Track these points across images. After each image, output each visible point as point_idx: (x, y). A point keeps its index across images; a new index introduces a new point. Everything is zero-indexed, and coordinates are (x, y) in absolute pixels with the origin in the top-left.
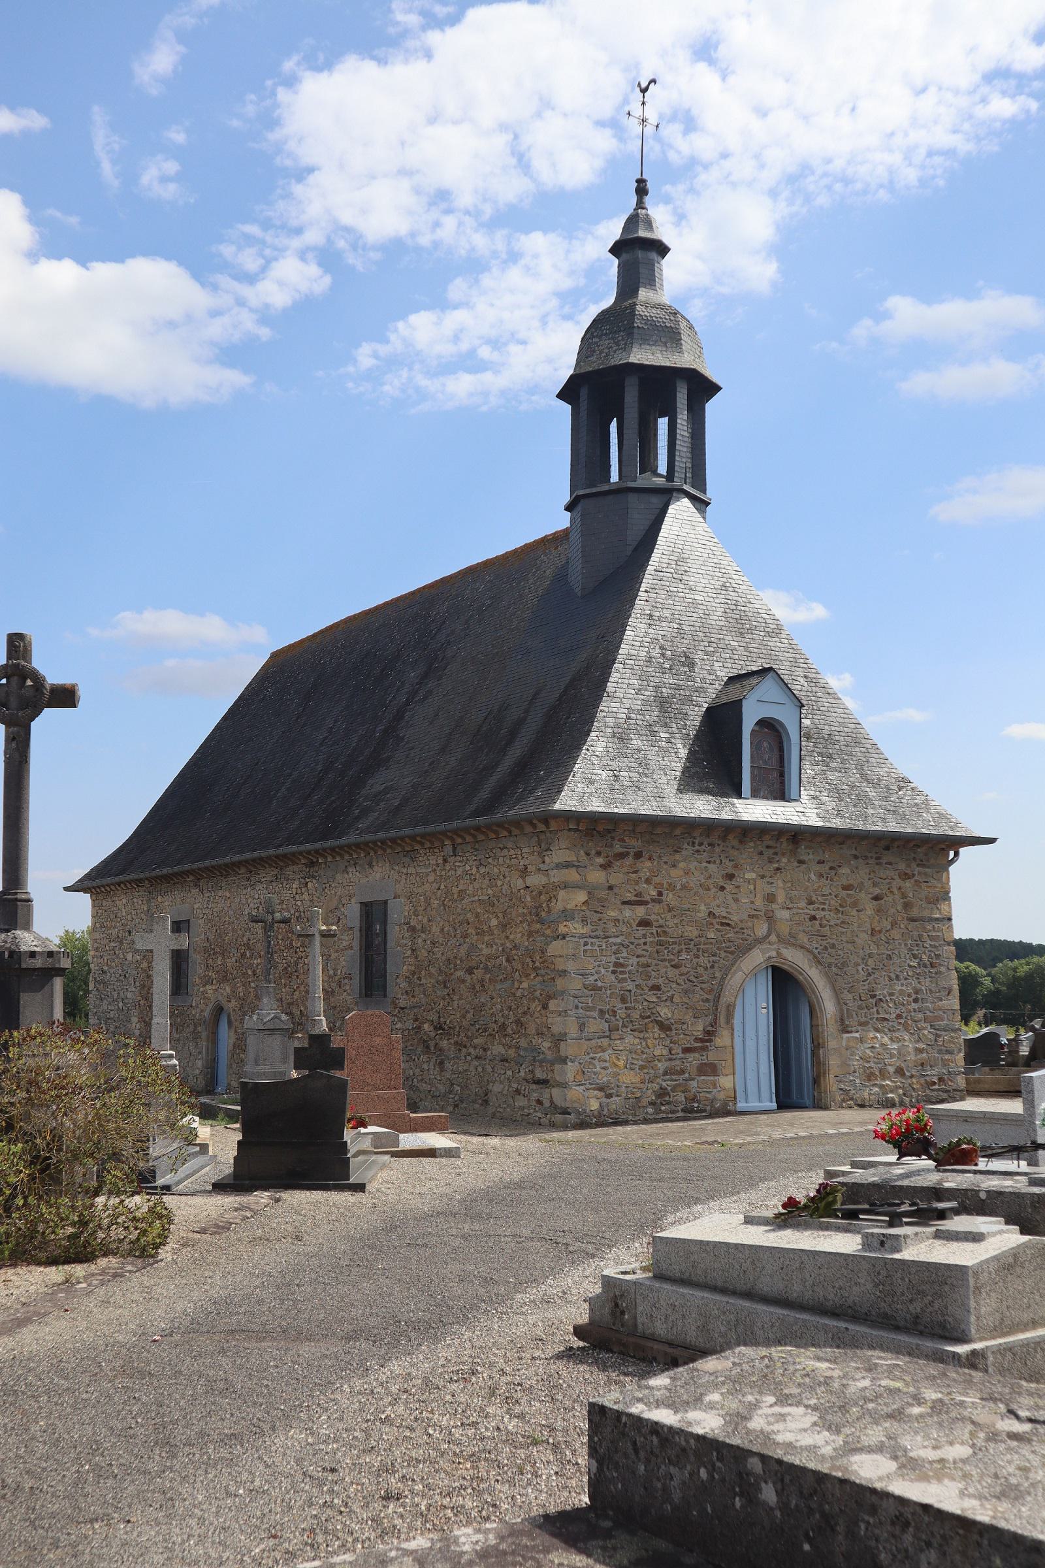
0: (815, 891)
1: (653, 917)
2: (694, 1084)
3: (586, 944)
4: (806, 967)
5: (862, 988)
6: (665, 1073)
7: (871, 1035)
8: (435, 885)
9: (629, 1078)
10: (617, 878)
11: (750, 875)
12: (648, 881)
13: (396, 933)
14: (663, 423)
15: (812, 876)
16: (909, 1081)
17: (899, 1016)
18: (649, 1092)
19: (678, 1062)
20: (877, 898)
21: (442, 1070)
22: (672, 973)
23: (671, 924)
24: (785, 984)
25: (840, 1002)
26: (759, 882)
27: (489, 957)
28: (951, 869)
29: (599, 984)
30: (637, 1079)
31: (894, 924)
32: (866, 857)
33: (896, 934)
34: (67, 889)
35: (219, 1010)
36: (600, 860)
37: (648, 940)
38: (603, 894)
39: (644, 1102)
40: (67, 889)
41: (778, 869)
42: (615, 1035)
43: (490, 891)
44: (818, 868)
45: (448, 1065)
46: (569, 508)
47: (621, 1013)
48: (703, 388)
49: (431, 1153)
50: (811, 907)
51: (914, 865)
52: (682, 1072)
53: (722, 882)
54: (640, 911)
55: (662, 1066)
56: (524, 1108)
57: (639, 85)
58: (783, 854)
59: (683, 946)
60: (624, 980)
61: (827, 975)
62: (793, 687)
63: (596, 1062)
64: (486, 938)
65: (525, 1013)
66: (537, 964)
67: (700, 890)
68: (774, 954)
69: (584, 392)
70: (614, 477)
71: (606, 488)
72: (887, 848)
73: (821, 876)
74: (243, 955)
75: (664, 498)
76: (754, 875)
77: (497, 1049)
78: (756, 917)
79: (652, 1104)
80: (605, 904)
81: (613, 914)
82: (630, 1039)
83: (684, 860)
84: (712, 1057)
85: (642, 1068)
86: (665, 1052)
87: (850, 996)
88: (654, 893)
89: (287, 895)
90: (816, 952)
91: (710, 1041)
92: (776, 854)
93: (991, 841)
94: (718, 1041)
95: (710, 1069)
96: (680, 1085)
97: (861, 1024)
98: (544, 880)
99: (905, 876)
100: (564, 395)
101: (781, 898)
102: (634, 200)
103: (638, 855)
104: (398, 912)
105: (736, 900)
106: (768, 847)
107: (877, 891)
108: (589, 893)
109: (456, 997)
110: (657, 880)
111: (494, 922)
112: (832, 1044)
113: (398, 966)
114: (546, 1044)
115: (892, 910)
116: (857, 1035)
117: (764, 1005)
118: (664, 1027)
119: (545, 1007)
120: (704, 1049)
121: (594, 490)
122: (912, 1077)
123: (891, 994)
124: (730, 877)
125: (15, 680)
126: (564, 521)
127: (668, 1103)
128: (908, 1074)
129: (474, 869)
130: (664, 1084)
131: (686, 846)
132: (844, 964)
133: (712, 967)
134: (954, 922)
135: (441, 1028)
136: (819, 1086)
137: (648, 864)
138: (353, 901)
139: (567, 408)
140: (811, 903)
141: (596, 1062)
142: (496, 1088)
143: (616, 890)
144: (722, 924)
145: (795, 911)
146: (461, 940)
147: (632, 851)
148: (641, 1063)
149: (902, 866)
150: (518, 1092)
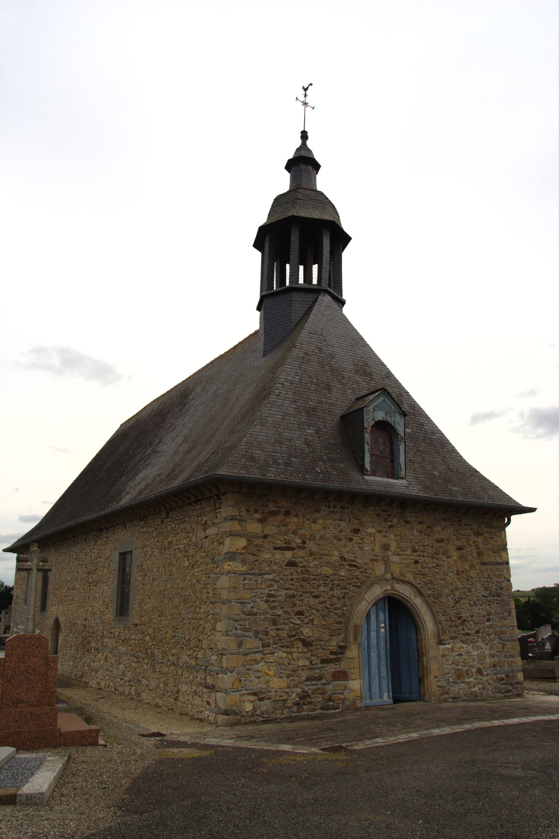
5: (452, 612)
9: (278, 683)
10: (271, 529)
12: (294, 533)
14: (315, 268)
20: (459, 548)
22: (313, 601)
27: (182, 589)
30: (285, 685)
36: (257, 516)
42: (267, 650)
45: (158, 669)
47: (273, 633)
52: (320, 678)
54: (288, 555)
55: (304, 675)
88: (299, 541)
103: (287, 513)
104: (137, 557)
111: (187, 564)
112: (432, 653)
114: (214, 657)
118: (306, 644)
119: (214, 629)
132: (439, 595)
137: (295, 520)
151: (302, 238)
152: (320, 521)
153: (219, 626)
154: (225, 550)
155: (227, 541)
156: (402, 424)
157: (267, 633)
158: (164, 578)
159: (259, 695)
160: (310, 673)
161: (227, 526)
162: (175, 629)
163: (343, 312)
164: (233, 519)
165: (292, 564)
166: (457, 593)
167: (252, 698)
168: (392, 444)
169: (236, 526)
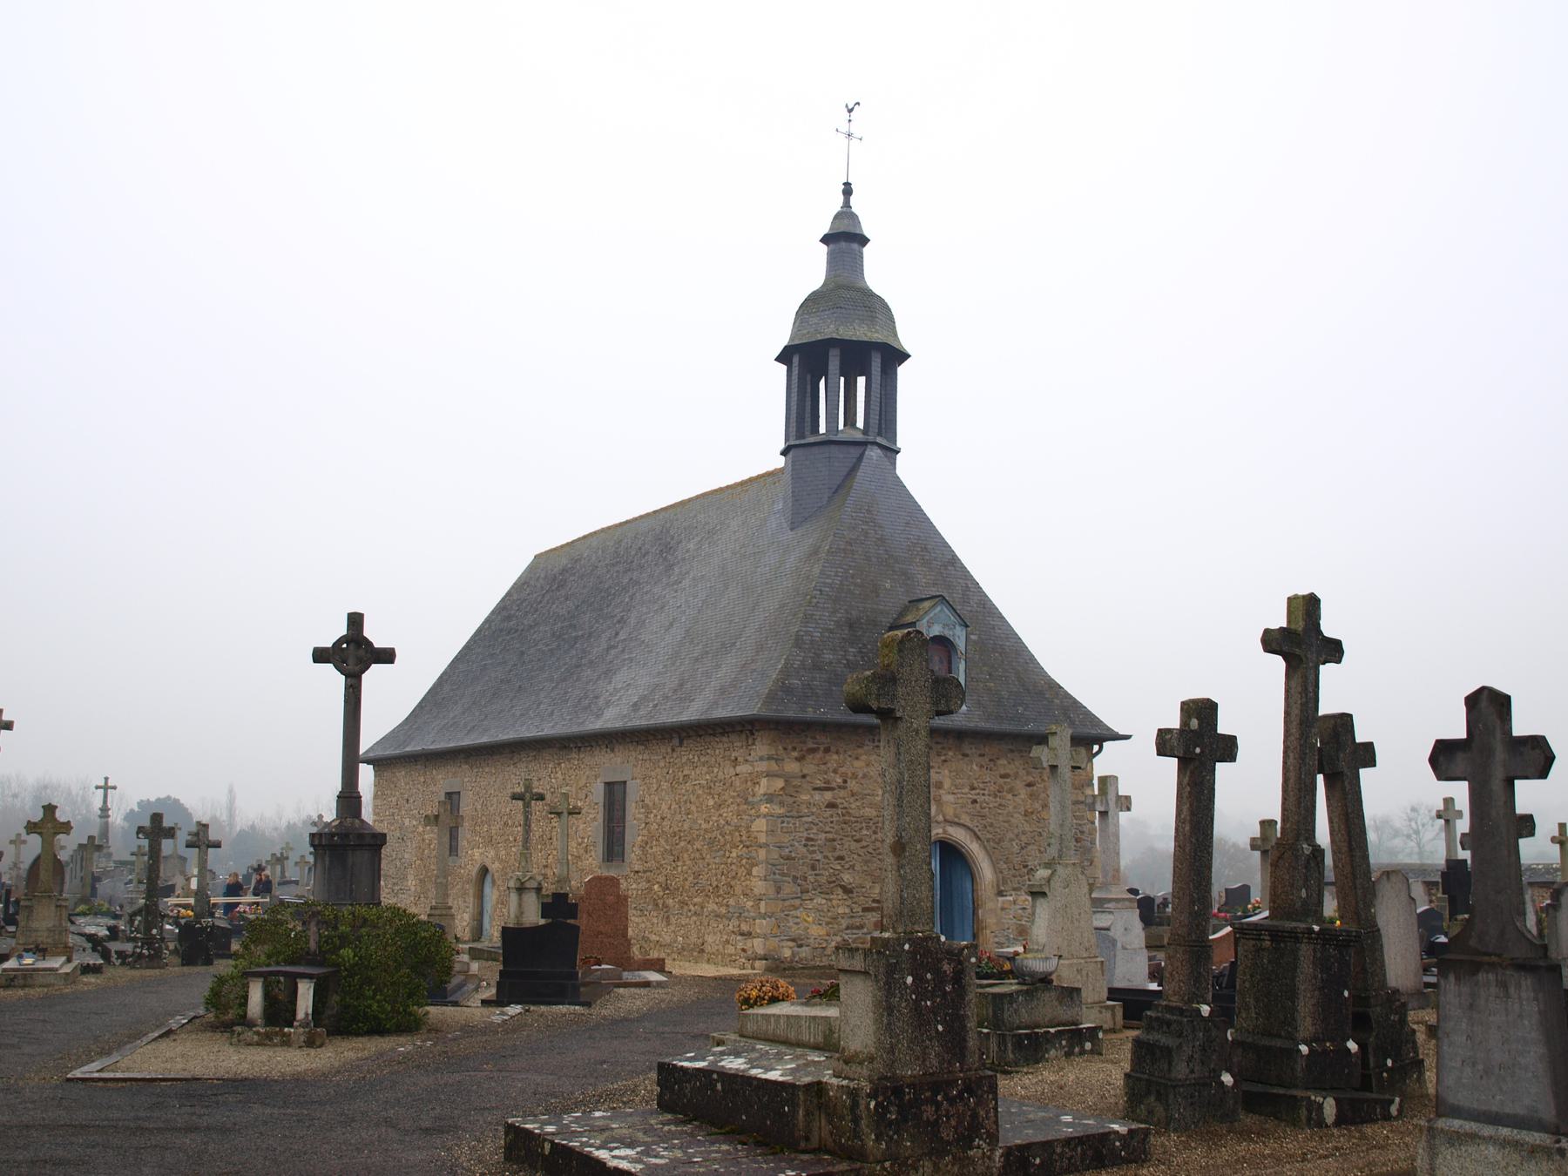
5: (1017, 860)
9: (816, 931)
10: (809, 768)
12: (835, 771)
13: (633, 812)
14: (861, 381)
20: (1029, 785)
21: (668, 924)
22: (854, 845)
27: (706, 830)
30: (823, 932)
35: (484, 871)
36: (795, 754)
38: (797, 782)
39: (829, 951)
42: (805, 896)
45: (673, 920)
46: (784, 453)
47: (811, 878)
49: (647, 984)
52: (862, 927)
54: (828, 796)
55: (844, 923)
69: (796, 360)
74: (506, 824)
77: (711, 906)
82: (819, 900)
88: (839, 780)
89: (544, 773)
102: (841, 198)
103: (827, 750)
104: (634, 791)
111: (711, 803)
112: (990, 905)
113: (634, 835)
114: (750, 903)
118: (847, 890)
119: (749, 873)
132: (1001, 840)
137: (835, 757)
142: (710, 939)
151: (843, 353)
152: (864, 757)
153: (755, 871)
154: (762, 791)
155: (764, 781)
156: (963, 638)
157: (805, 879)
158: (678, 817)
159: (798, 942)
160: (850, 921)
161: (762, 766)
162: (697, 875)
163: (899, 472)
164: (770, 758)
165: (831, 805)
166: (1023, 838)
167: (791, 944)
168: (950, 662)
169: (774, 766)
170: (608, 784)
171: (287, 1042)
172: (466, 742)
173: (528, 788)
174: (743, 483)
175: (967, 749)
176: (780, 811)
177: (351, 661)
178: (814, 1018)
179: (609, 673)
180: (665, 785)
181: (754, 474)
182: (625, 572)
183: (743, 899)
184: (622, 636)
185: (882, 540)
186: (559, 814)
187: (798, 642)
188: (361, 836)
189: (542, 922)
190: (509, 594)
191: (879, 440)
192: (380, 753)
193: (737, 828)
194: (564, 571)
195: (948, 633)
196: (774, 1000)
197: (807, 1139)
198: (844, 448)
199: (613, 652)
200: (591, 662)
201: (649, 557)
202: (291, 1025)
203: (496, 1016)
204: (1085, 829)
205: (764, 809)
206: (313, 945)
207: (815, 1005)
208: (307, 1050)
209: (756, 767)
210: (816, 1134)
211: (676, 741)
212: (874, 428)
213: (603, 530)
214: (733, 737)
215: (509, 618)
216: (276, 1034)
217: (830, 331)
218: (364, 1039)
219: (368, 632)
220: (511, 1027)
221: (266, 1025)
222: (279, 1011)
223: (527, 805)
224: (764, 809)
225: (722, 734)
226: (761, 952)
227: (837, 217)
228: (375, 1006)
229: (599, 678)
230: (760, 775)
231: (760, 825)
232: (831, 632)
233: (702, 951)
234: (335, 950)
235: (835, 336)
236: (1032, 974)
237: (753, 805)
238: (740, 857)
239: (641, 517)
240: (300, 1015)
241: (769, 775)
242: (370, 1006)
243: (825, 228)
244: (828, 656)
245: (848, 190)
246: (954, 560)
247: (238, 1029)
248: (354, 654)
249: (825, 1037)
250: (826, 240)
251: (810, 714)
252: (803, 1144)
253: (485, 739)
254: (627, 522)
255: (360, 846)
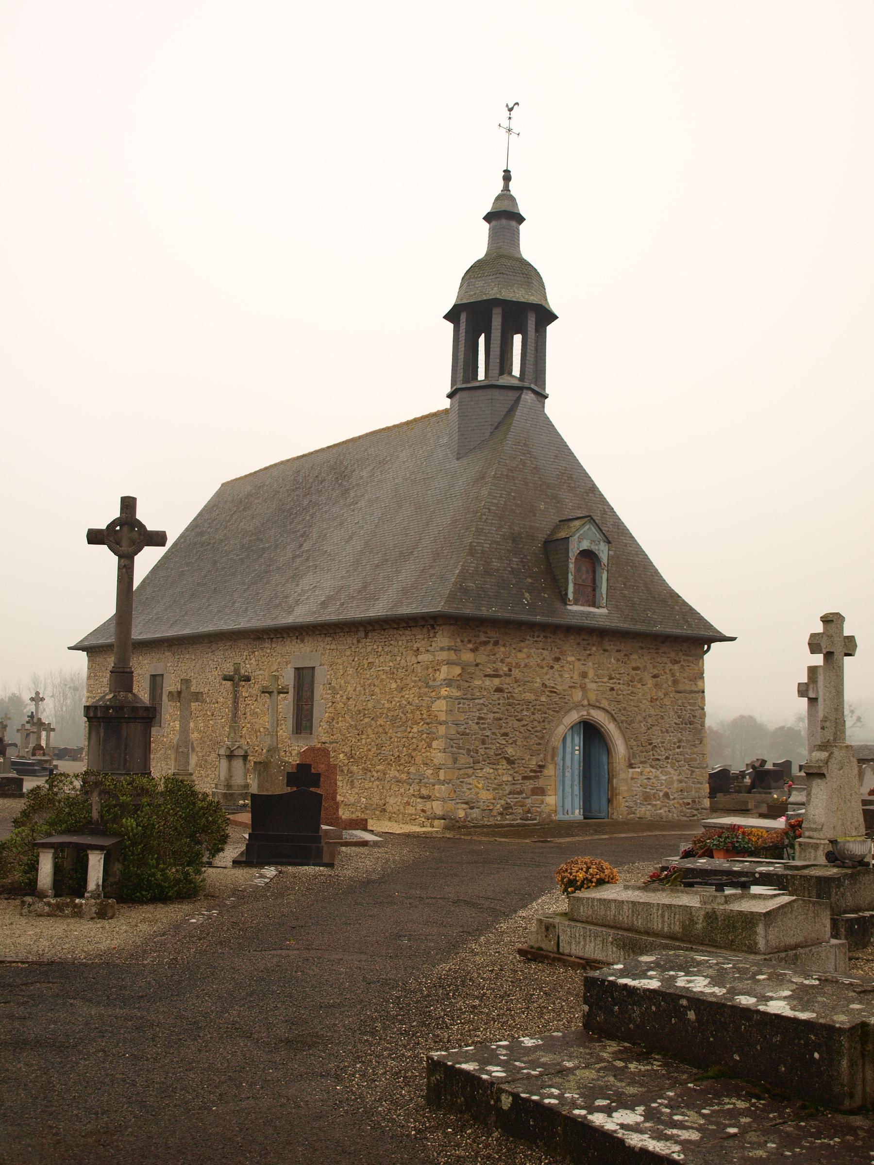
0: (614, 671)
1: (505, 686)
2: (529, 801)
3: (459, 704)
4: (607, 723)
5: (644, 738)
6: (510, 793)
7: (648, 770)
8: (351, 658)
9: (485, 795)
10: (482, 658)
11: (571, 659)
12: (502, 661)
13: (320, 692)
14: (518, 339)
15: (612, 660)
16: (672, 802)
17: (667, 758)
18: (499, 806)
19: (519, 786)
20: (655, 676)
21: (353, 787)
22: (517, 724)
23: (516, 691)
24: (591, 732)
25: (629, 747)
26: (577, 664)
27: (389, 709)
28: (705, 657)
29: (468, 731)
30: (491, 797)
31: (666, 694)
32: (649, 648)
33: (667, 701)
34: (70, 648)
36: (470, 646)
37: (501, 702)
38: (471, 669)
39: (495, 813)
40: (70, 648)
41: (590, 655)
42: (477, 766)
43: (391, 664)
44: (616, 654)
45: (357, 784)
46: (450, 396)
47: (482, 751)
48: (547, 316)
49: (365, 844)
50: (611, 681)
51: (681, 654)
53: (551, 663)
54: (496, 682)
55: (508, 789)
56: (412, 815)
57: (507, 106)
58: (594, 645)
59: (525, 707)
60: (484, 729)
61: (620, 728)
62: (603, 528)
63: (464, 785)
64: (387, 697)
65: (414, 750)
66: (424, 716)
67: (537, 669)
68: (585, 713)
69: (463, 317)
70: (481, 376)
71: (477, 384)
72: (663, 642)
73: (618, 660)
75: (519, 392)
76: (573, 659)
77: (393, 773)
78: (574, 687)
79: (501, 814)
80: (473, 676)
81: (478, 683)
82: (488, 770)
83: (527, 647)
84: (540, 783)
85: (494, 789)
86: (510, 779)
87: (635, 743)
88: (506, 669)
90: (613, 712)
91: (541, 772)
92: (589, 644)
93: (733, 639)
94: (546, 772)
95: (540, 791)
96: (519, 802)
97: (641, 763)
98: (431, 658)
99: (675, 662)
100: (449, 317)
101: (591, 674)
102: (501, 183)
103: (496, 643)
105: (561, 676)
106: (584, 640)
107: (656, 672)
108: (463, 668)
109: (363, 737)
110: (508, 660)
111: (394, 686)
112: (622, 775)
113: (321, 712)
115: (665, 685)
116: (639, 770)
117: (577, 748)
118: (510, 762)
119: (430, 746)
120: (537, 777)
121: (469, 385)
122: (674, 799)
123: (663, 743)
124: (557, 659)
125: (126, 528)
126: (446, 404)
127: (511, 814)
128: (672, 797)
129: (380, 648)
130: (509, 801)
131: (528, 637)
132: (632, 722)
133: (544, 721)
134: (706, 694)
135: (352, 757)
136: (612, 804)
137: (502, 649)
138: (289, 666)
139: (450, 326)
140: (611, 678)
141: (464, 785)
142: (391, 801)
143: (480, 667)
144: (551, 692)
145: (600, 684)
146: (369, 698)
147: (492, 640)
148: (494, 786)
149: (673, 655)
150: (408, 803)
151: (501, 313)
153: (435, 744)
155: (444, 669)
157: (477, 752)
159: (470, 804)
160: (512, 787)
161: (443, 656)
162: (380, 747)
163: (547, 411)
164: (450, 649)
166: (649, 720)
168: (594, 572)
169: (453, 656)
170: (297, 669)
171: (78, 913)
172: (171, 633)
173: (237, 670)
174: (408, 423)
175: (607, 645)
176: (457, 693)
177: (125, 543)
178: (669, 906)
179: (296, 577)
180: (350, 671)
181: (419, 415)
182: (305, 495)
183: (423, 768)
184: (306, 547)
185: (536, 468)
186: (270, 693)
187: (472, 552)
188: (135, 709)
189: (289, 790)
190: (200, 514)
191: (533, 386)
192: (94, 642)
193: (418, 708)
194: (249, 495)
195: (594, 548)
196: (601, 882)
197: (852, 1096)
198: (504, 392)
199: (298, 560)
200: (278, 568)
201: (326, 484)
202: (82, 896)
203: (242, 875)
204: (697, 713)
205: (444, 692)
206: (95, 815)
207: (655, 890)
208: (100, 924)
209: (438, 654)
210: (859, 1088)
211: (361, 634)
212: (529, 376)
213: (282, 463)
214: (415, 631)
215: (202, 534)
216: (67, 905)
217: (494, 292)
218: (150, 908)
219: (142, 515)
220: (276, 890)
221: (56, 895)
222: (70, 881)
223: (235, 686)
224: (444, 692)
225: (405, 628)
226: (439, 812)
227: (498, 198)
228: (159, 876)
229: (287, 581)
230: (440, 663)
231: (440, 705)
232: (498, 543)
233: (385, 810)
234: (116, 819)
235: (498, 296)
236: (852, 857)
237: (433, 689)
238: (421, 732)
239: (316, 452)
240: (91, 886)
241: (449, 663)
242: (154, 875)
243: (488, 208)
244: (496, 564)
245: (507, 177)
246: (593, 489)
247: (29, 899)
248: (124, 534)
249: (684, 927)
250: (488, 218)
251: (484, 612)
252: (847, 1102)
253: (186, 631)
254: (304, 456)
255: (133, 719)
